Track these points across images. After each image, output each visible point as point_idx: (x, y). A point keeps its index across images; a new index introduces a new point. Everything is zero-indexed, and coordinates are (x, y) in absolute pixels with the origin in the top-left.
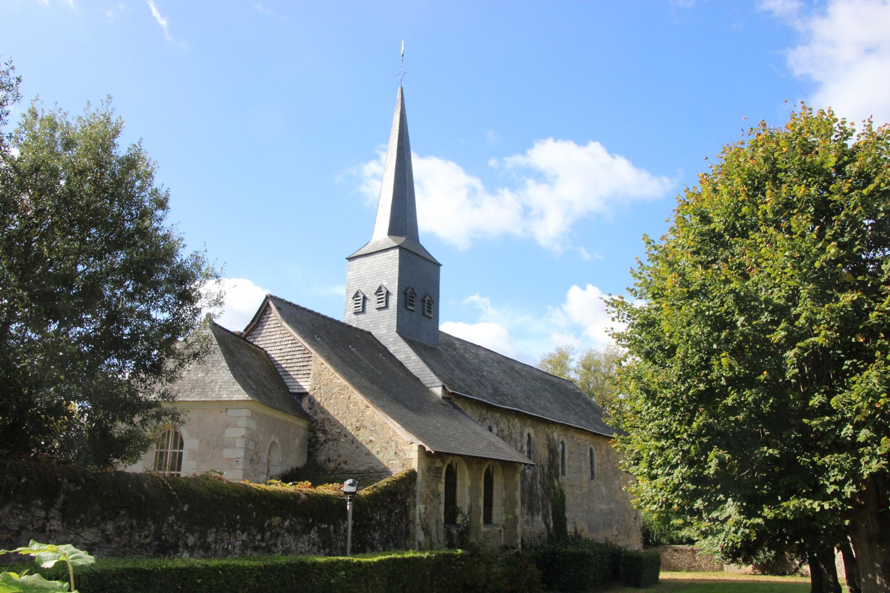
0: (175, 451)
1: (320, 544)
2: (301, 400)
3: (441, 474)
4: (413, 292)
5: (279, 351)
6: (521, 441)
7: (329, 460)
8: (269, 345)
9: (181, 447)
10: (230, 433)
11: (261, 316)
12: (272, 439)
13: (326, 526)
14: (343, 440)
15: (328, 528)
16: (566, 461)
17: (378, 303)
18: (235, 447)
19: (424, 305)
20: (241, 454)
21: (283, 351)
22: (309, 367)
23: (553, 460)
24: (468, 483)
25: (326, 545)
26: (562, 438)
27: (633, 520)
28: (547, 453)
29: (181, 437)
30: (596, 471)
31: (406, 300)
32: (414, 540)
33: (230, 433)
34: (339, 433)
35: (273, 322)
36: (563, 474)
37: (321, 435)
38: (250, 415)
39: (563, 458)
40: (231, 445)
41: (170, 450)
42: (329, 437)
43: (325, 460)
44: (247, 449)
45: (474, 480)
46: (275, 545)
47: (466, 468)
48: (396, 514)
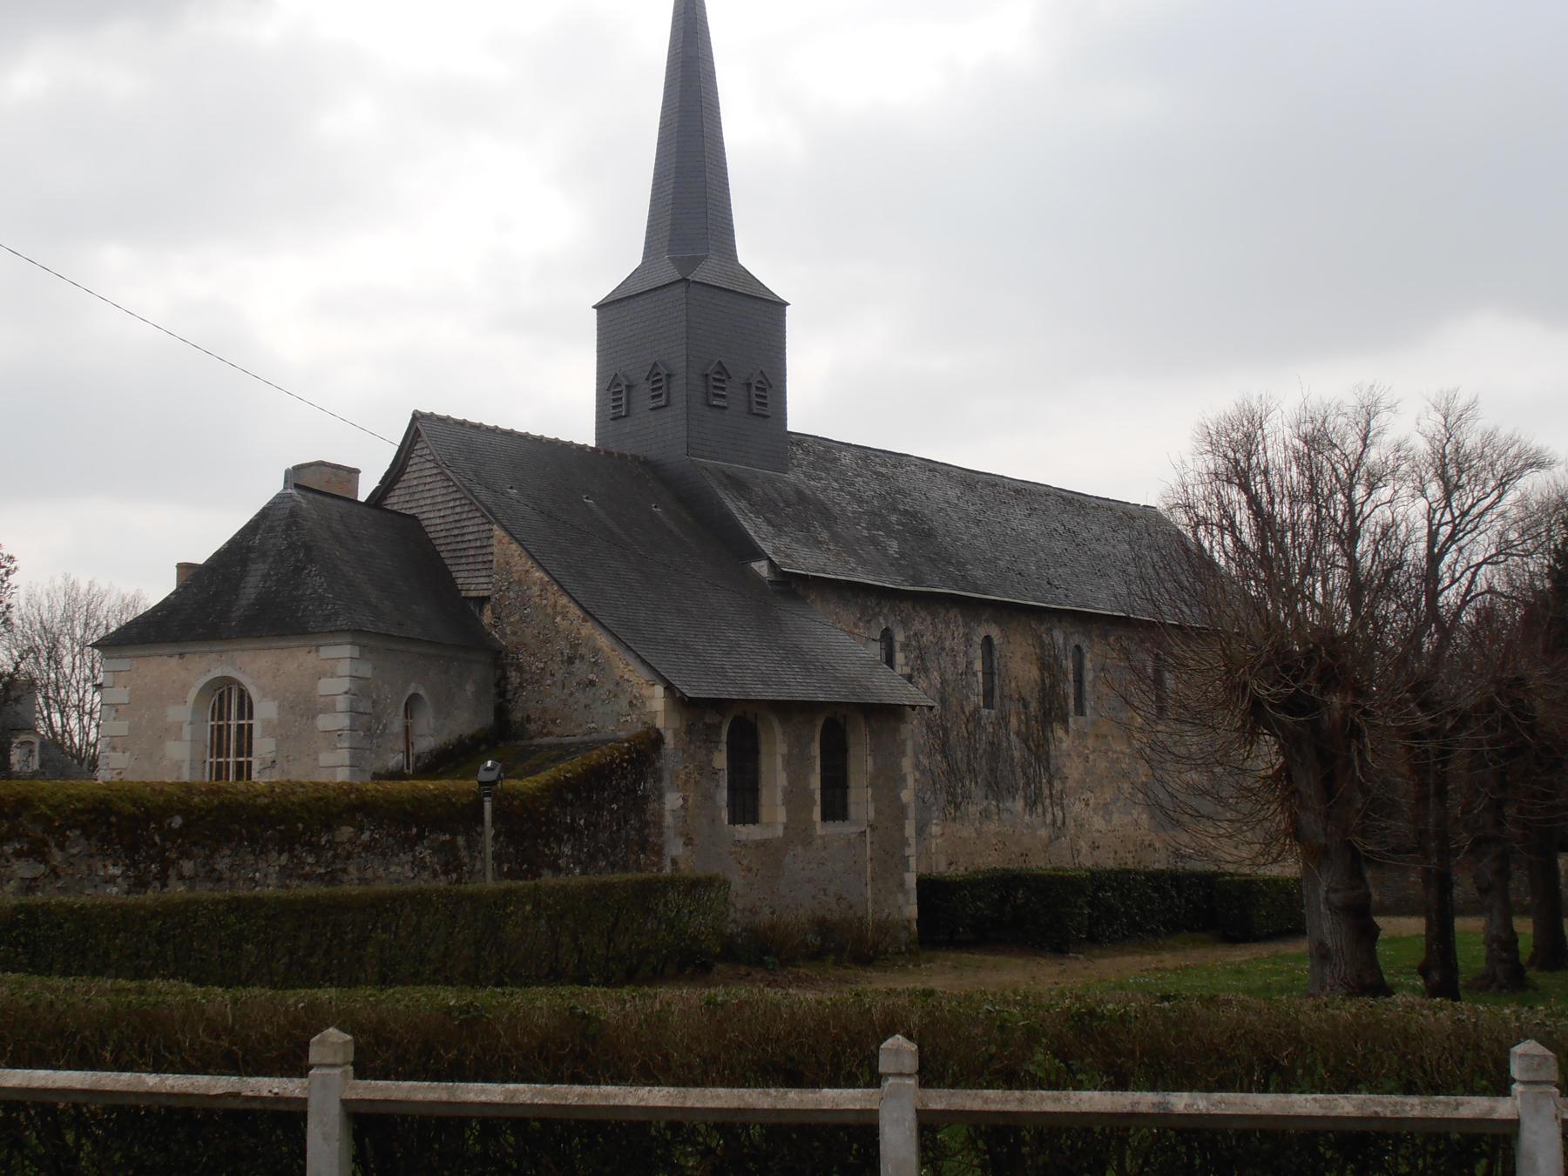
1: (438, 867)
2: (481, 610)
3: (719, 735)
5: (441, 521)
6: (966, 653)
7: (529, 719)
8: (425, 509)
9: (251, 717)
10: (327, 686)
13: (447, 837)
14: (549, 682)
15: (453, 842)
16: (1088, 687)
17: (653, 397)
20: (343, 721)
21: (447, 520)
22: (489, 550)
23: (1053, 686)
24: (781, 748)
25: (450, 867)
26: (1076, 639)
28: (1035, 673)
29: (249, 694)
31: (707, 387)
33: (327, 686)
34: (542, 669)
35: (414, 468)
36: (1080, 710)
37: (514, 673)
38: (357, 655)
39: (1079, 681)
40: (330, 708)
41: (234, 723)
42: (527, 676)
43: (522, 718)
44: (354, 712)
46: (344, 871)
48: (611, 811)
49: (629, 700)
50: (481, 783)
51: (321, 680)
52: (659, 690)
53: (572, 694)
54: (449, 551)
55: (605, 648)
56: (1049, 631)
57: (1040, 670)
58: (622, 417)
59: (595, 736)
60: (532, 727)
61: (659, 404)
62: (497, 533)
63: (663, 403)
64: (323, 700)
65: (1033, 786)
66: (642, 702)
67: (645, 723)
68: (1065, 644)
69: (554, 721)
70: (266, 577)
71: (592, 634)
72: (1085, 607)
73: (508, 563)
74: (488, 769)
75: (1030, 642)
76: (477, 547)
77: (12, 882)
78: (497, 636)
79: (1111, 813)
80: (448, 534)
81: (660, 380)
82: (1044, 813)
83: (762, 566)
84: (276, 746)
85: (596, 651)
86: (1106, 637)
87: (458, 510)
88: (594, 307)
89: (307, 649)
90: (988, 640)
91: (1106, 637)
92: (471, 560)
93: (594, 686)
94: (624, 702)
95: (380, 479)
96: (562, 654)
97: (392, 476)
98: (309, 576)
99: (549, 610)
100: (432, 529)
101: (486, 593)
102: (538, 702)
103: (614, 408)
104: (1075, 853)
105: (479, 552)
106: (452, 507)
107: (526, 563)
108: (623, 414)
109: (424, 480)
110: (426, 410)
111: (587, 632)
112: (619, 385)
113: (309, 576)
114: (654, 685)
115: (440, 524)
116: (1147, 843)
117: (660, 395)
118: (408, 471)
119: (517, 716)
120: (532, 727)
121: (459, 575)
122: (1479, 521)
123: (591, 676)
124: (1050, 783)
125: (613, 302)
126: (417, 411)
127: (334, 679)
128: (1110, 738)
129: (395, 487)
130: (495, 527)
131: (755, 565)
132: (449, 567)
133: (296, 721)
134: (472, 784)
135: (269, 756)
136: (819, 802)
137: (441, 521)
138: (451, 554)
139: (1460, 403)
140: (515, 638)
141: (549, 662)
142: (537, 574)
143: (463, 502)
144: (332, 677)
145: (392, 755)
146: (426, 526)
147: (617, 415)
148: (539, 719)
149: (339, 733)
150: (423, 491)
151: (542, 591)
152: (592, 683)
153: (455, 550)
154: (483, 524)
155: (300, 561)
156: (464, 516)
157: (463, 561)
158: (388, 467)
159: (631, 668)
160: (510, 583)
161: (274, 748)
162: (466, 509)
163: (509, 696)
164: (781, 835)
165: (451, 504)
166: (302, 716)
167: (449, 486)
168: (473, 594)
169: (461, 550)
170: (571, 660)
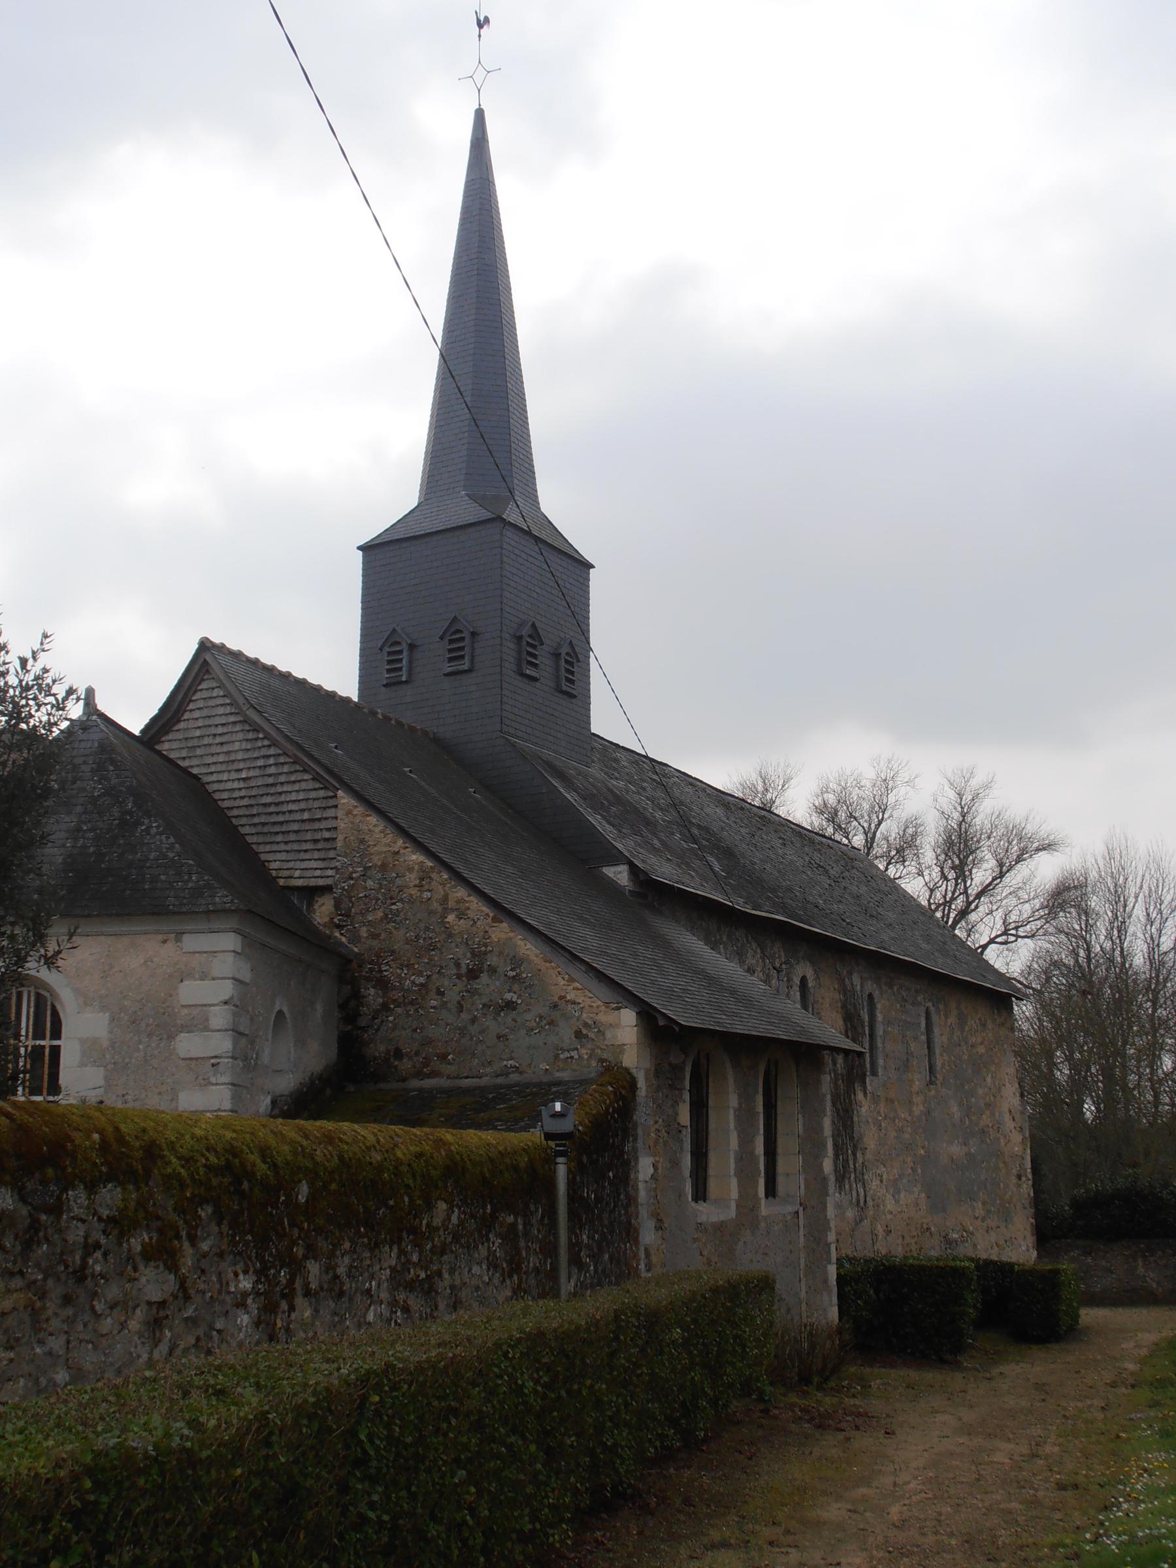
0: (43, 1043)
2: (310, 904)
4: (535, 633)
5: (242, 785)
7: (398, 1054)
8: (213, 769)
9: (57, 1033)
10: (191, 992)
11: (186, 694)
12: (277, 1008)
14: (434, 1003)
17: (451, 660)
18: (207, 1029)
19: (557, 669)
20: (222, 1044)
21: (253, 783)
24: (733, 1101)
26: (870, 986)
27: (1014, 1180)
30: (939, 1064)
31: (519, 652)
32: (636, 1241)
33: (191, 992)
34: (422, 985)
35: (197, 714)
36: (874, 1073)
37: (372, 991)
40: (199, 1024)
43: (388, 1052)
45: (746, 1096)
47: (728, 1065)
49: (575, 1028)
50: (549, 1136)
51: (186, 983)
52: (629, 1017)
53: (474, 1020)
54: (255, 825)
55: (532, 957)
56: (850, 973)
57: (844, 1020)
58: (402, 682)
59: (514, 1078)
60: (405, 1065)
61: (461, 668)
62: (345, 801)
63: (466, 667)
64: (186, 1011)
65: (841, 1158)
66: (599, 1031)
67: (602, 1060)
68: (861, 991)
69: (443, 1057)
70: (75, 833)
71: (510, 938)
72: (885, 949)
73: (362, 841)
74: (556, 1115)
75: (836, 986)
76: (303, 821)
77: (138, 1311)
78: (344, 939)
79: (899, 1192)
80: (252, 802)
81: (463, 639)
82: (851, 1189)
83: (620, 872)
84: (106, 1078)
85: (517, 962)
86: (891, 987)
87: (272, 770)
88: (359, 548)
89: (160, 937)
90: (804, 980)
91: (891, 987)
92: (292, 837)
93: (514, 1009)
94: (566, 1033)
95: (142, 727)
96: (458, 965)
97: (160, 724)
98: (149, 834)
99: (435, 905)
100: (225, 795)
101: (329, 882)
102: (415, 1030)
103: (389, 671)
104: (874, 1237)
105: (307, 826)
106: (260, 767)
107: (395, 842)
108: (404, 679)
109: (213, 731)
110: (216, 639)
111: (503, 936)
112: (398, 643)
113: (149, 834)
114: (618, 1009)
115: (240, 789)
116: (925, 1226)
117: (462, 657)
118: (185, 717)
119: (378, 1049)
120: (405, 1065)
121: (270, 857)
122: (979, 902)
123: (508, 996)
124: (854, 1154)
125: (391, 542)
126: (207, 638)
127: (206, 982)
128: (896, 1103)
129: (163, 739)
130: (340, 793)
131: (609, 871)
132: (254, 846)
133: (140, 1042)
134: (534, 1136)
135: (93, 1093)
136: (763, 1174)
137: (242, 785)
138: (259, 829)
139: (974, 783)
140: (375, 943)
141: (435, 976)
142: (414, 857)
143: (282, 760)
144: (202, 980)
145: (262, 1098)
146: (214, 792)
147: (393, 680)
148: (417, 1054)
149: (212, 1061)
150: (210, 745)
151: (422, 879)
152: (510, 1006)
153: (264, 824)
154: (315, 789)
155: (130, 813)
156: (283, 779)
157: (279, 838)
158: (156, 712)
159: (577, 985)
160: (366, 869)
161: (102, 1082)
162: (286, 769)
163: (363, 1022)
164: (734, 1216)
165: (261, 763)
166: (150, 1035)
167: (257, 739)
168: (299, 883)
169: (274, 823)
170: (473, 974)
